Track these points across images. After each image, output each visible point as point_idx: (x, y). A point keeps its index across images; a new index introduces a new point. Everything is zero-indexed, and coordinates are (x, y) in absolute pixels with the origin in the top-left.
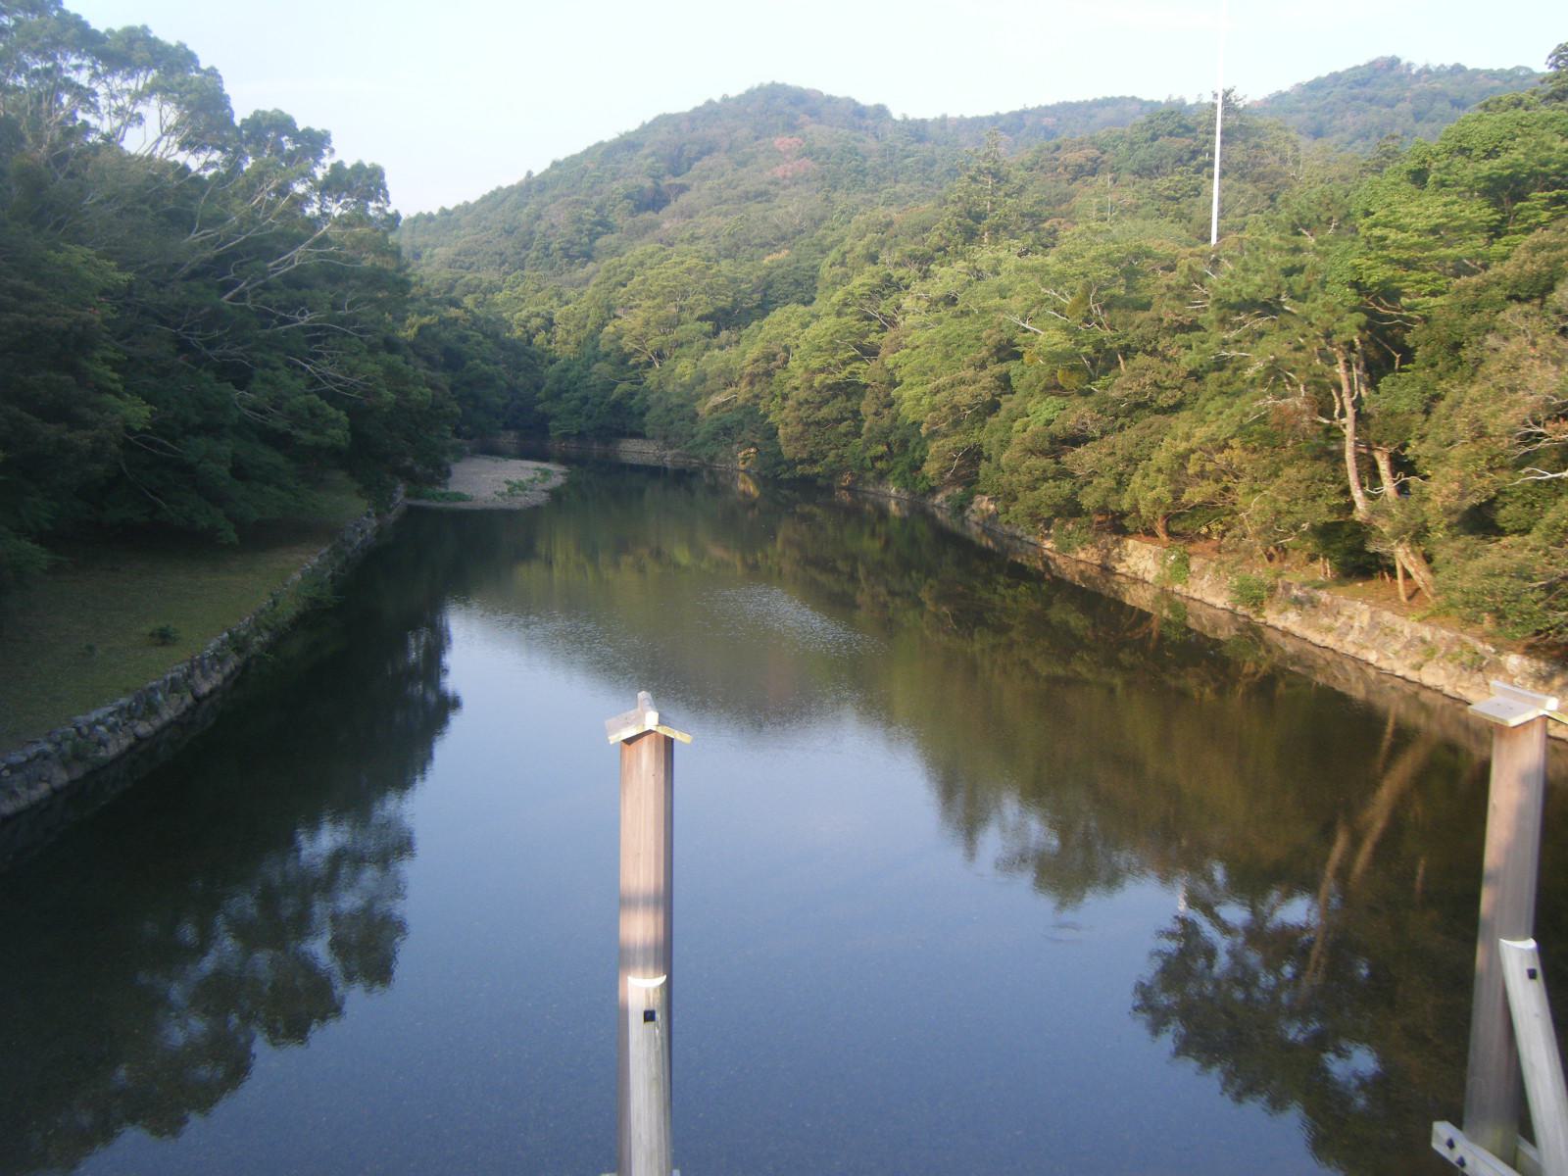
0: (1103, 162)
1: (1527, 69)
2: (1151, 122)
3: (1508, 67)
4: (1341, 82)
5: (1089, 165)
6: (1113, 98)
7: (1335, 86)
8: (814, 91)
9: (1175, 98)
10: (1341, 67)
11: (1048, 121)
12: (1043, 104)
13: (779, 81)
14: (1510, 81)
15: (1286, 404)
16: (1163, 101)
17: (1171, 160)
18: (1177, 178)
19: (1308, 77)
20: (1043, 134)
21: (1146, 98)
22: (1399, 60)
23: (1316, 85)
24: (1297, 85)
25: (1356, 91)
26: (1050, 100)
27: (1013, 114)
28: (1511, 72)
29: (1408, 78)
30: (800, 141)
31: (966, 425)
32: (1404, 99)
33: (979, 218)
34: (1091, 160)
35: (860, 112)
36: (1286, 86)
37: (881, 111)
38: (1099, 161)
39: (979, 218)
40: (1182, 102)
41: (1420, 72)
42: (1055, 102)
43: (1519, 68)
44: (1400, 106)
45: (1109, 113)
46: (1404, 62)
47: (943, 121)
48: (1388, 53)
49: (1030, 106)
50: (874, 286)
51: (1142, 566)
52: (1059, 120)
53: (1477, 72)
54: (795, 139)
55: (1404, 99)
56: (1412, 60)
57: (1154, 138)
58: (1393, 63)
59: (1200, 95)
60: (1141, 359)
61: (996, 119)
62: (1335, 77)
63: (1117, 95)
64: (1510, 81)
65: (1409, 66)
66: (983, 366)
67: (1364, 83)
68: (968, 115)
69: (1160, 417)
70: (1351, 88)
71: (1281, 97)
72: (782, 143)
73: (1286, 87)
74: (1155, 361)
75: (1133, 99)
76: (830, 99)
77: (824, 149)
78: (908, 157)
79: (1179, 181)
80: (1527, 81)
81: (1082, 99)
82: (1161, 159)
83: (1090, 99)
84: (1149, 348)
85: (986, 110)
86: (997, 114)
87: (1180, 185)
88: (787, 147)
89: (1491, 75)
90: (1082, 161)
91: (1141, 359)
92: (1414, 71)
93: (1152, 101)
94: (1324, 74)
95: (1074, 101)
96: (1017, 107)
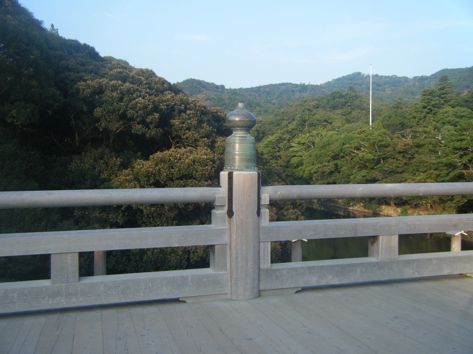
0: (320, 105)
1: (396, 76)
2: (333, 94)
3: (390, 75)
4: (346, 79)
5: (317, 106)
6: (284, 83)
7: (344, 80)
8: (203, 81)
9: (302, 83)
10: (345, 74)
11: (267, 89)
12: (265, 85)
13: (193, 78)
14: (391, 79)
15: (469, 171)
16: (299, 84)
17: (341, 105)
18: (345, 110)
19: (336, 77)
20: (266, 93)
21: (294, 83)
22: (361, 73)
23: (339, 79)
24: (333, 80)
25: (350, 81)
26: (267, 83)
27: (257, 87)
28: (391, 77)
29: (364, 78)
30: (205, 96)
31: (325, 177)
32: (364, 84)
33: (305, 121)
34: (317, 104)
35: (217, 87)
36: (330, 80)
37: (223, 87)
38: (319, 104)
39: (305, 121)
40: (304, 84)
41: (367, 76)
42: (268, 84)
43: (394, 76)
44: (363, 86)
45: (284, 88)
46: (362, 73)
47: (241, 89)
48: (358, 71)
49: (261, 85)
50: (277, 139)
51: (390, 213)
52: (270, 89)
53: (382, 76)
54: (203, 95)
55: (364, 84)
56: (365, 73)
57: (334, 99)
58: (359, 74)
59: (309, 82)
60: (390, 160)
61: (252, 89)
62: (344, 78)
63: (286, 82)
64: (391, 79)
65: (363, 74)
66: (329, 162)
67: (352, 79)
68: (244, 87)
69: (399, 175)
70: (348, 81)
71: (329, 83)
72: (200, 96)
73: (330, 80)
74: (395, 160)
75: (290, 83)
76: (208, 83)
77: (213, 98)
78: (235, 100)
79: (345, 111)
80: (396, 79)
81: (276, 83)
82: (338, 105)
83: (278, 83)
84: (393, 157)
85: (249, 86)
86: (252, 87)
87: (346, 112)
88: (202, 97)
89: (385, 77)
90: (315, 104)
91: (390, 160)
92: (365, 76)
93: (295, 84)
94: (341, 77)
95: (274, 84)
96: (258, 85)
